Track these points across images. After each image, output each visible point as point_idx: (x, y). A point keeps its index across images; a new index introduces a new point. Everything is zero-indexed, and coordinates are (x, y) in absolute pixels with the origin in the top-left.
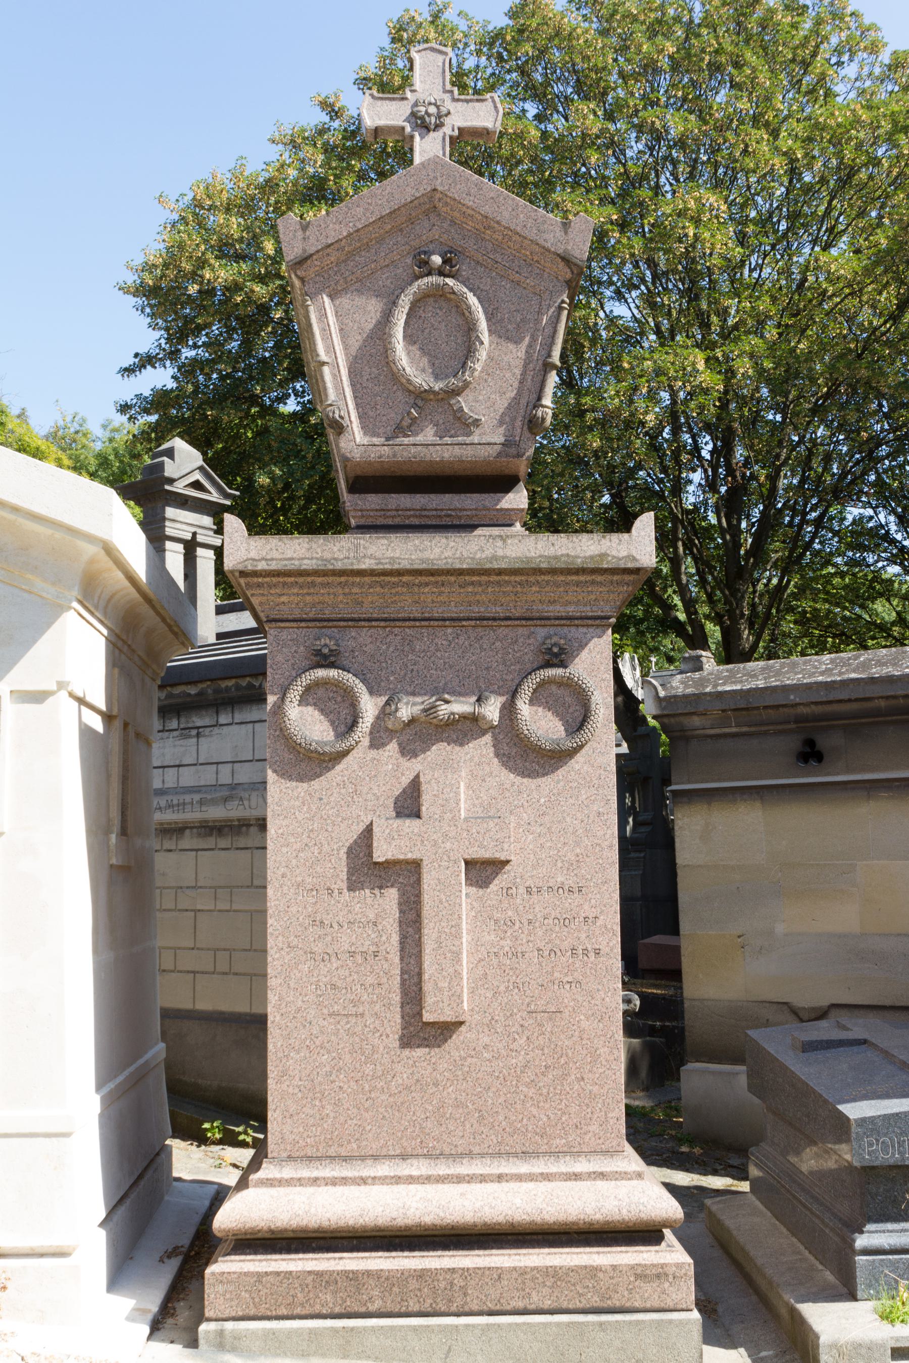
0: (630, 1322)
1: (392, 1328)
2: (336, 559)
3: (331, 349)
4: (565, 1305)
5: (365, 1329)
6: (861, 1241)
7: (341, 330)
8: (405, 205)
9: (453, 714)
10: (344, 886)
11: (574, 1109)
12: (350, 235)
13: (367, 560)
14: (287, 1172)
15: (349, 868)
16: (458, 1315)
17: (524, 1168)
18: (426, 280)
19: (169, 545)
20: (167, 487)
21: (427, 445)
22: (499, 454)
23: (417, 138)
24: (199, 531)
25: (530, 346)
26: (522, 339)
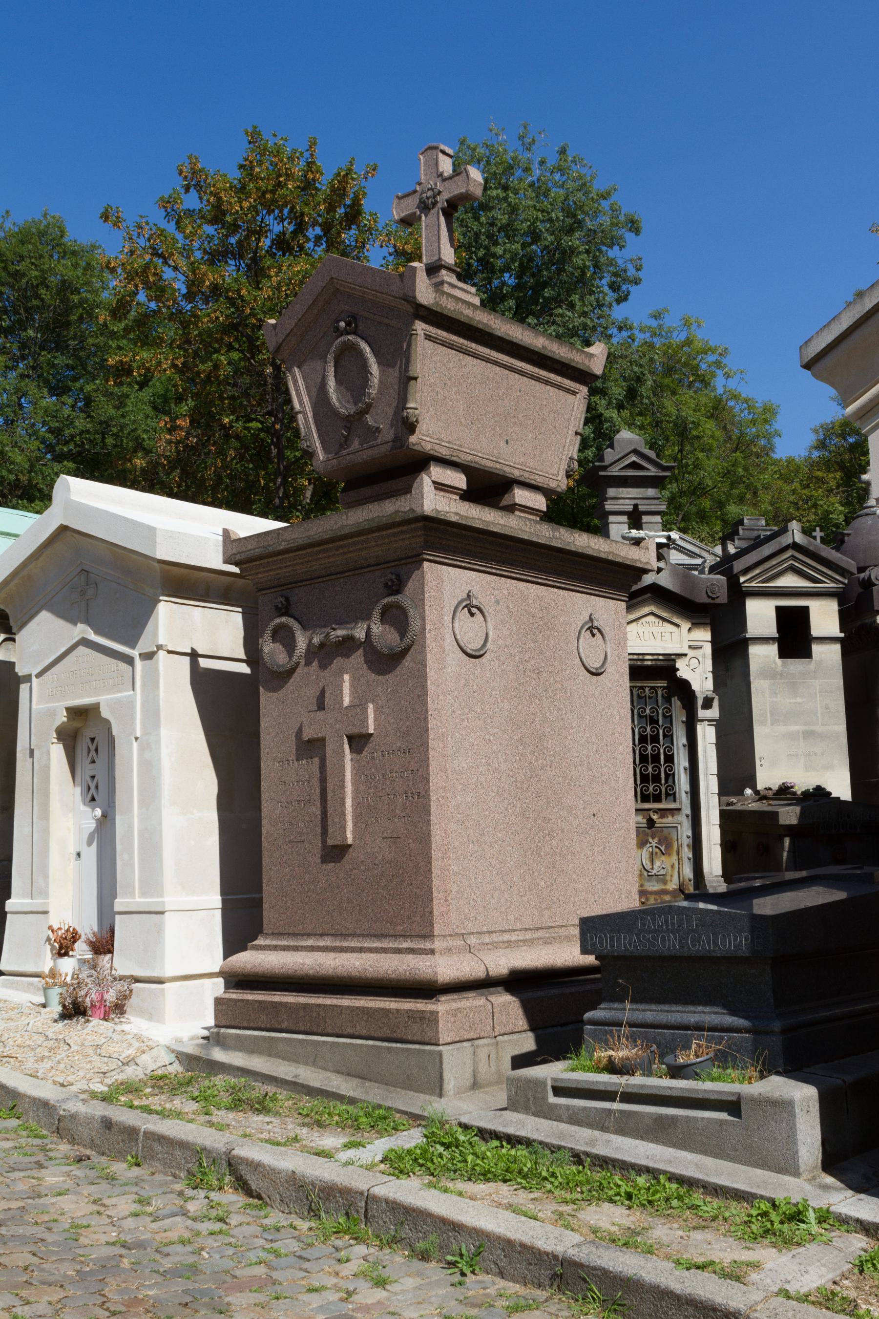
0: (403, 1049)
1: (290, 1039)
2: (269, 546)
3: (301, 402)
4: (373, 1034)
5: (278, 1038)
6: (587, 1015)
7: (306, 387)
8: (319, 294)
9: (338, 637)
10: (294, 758)
11: (407, 905)
12: (296, 325)
13: (283, 543)
14: (268, 942)
15: (297, 746)
16: (322, 1035)
17: (377, 944)
18: (339, 340)
19: (612, 518)
20: (601, 473)
21: (358, 452)
22: (392, 449)
23: (423, 218)
24: (638, 502)
25: (400, 367)
26: (396, 363)
